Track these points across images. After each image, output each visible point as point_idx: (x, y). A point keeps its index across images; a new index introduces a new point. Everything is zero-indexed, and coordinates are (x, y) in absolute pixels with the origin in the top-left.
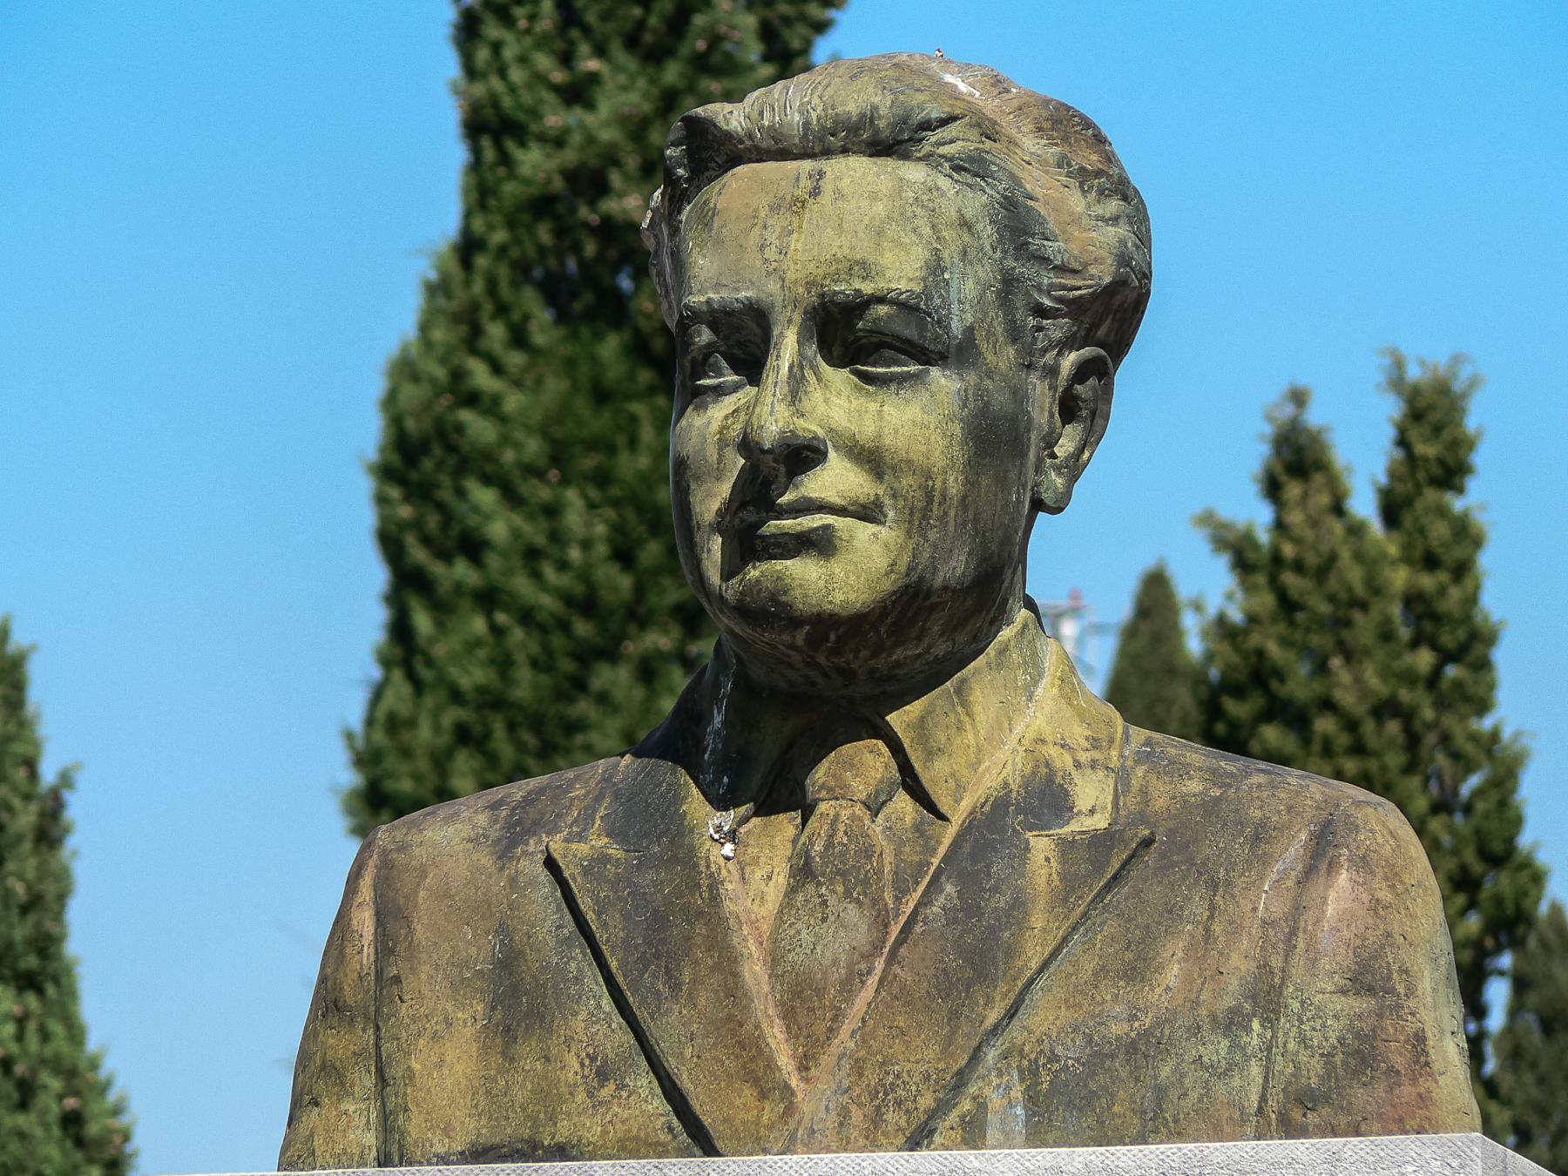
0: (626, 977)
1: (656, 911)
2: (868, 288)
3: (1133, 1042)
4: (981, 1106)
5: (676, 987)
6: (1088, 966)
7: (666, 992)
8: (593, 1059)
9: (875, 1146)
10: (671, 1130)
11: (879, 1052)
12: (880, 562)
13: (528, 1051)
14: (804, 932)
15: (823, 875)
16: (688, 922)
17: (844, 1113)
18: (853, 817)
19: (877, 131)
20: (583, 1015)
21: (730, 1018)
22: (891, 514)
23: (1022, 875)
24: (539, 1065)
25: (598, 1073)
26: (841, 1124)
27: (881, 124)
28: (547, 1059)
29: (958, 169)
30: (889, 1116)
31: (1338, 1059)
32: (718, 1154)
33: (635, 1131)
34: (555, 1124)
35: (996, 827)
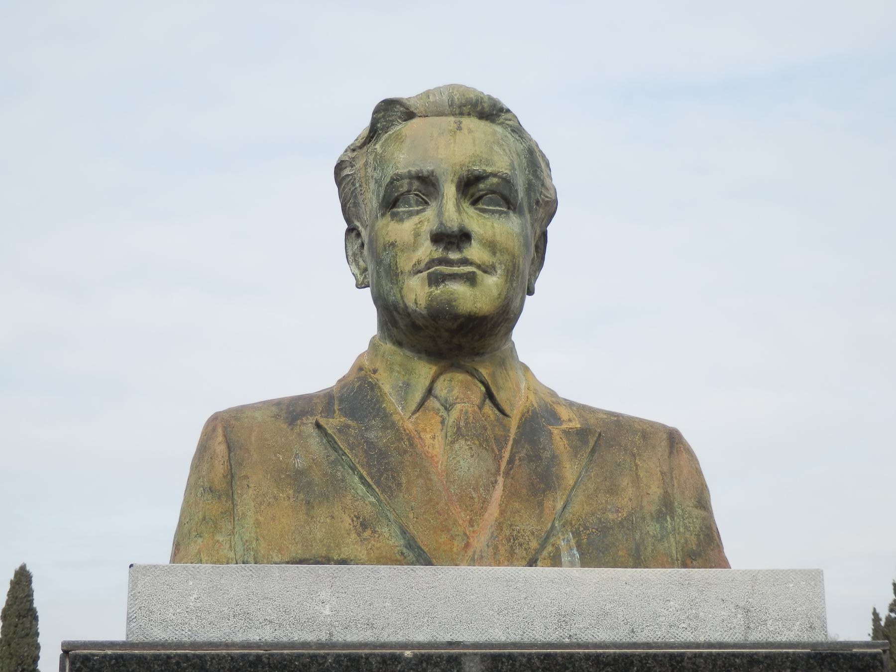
0: (372, 479)
1: (380, 450)
2: (489, 170)
3: (620, 522)
4: (558, 550)
5: (399, 485)
6: (591, 486)
7: (394, 487)
8: (358, 518)
9: (511, 564)
10: (402, 554)
11: (509, 519)
12: (495, 292)
13: (321, 512)
14: (462, 462)
15: (468, 435)
16: (400, 455)
17: (496, 548)
18: (474, 411)
19: (483, 108)
20: (349, 497)
21: (430, 500)
22: (499, 272)
23: (552, 444)
24: (328, 520)
25: (362, 524)
26: (495, 553)
27: (485, 105)
28: (333, 517)
29: (513, 131)
30: (517, 551)
31: (702, 536)
32: (432, 565)
33: (384, 554)
34: (340, 549)
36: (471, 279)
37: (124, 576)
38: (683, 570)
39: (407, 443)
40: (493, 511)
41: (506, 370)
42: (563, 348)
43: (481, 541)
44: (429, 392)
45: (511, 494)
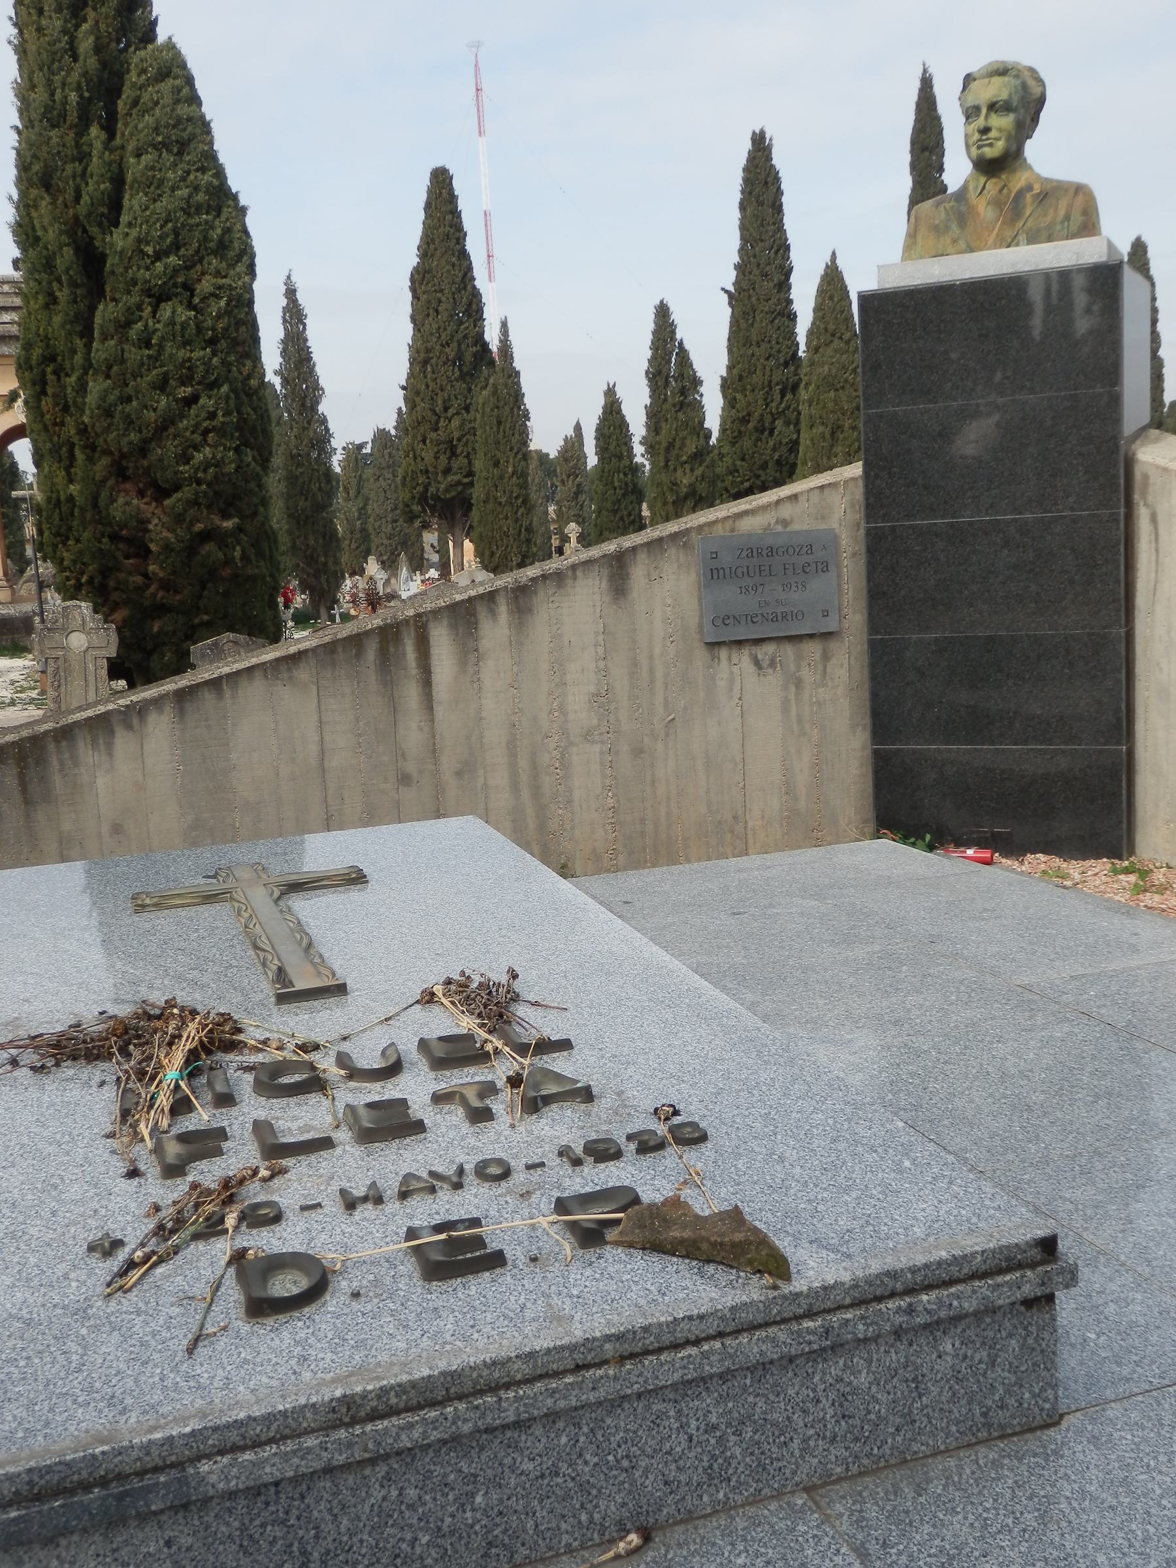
35: (1020, 194)
36: (991, 145)
37: (876, 269)
38: (811, 853)
39: (972, 209)
40: (996, 231)
41: (110, 754)
42: (1047, 155)
43: (990, 242)
44: (984, 188)
45: (1003, 223)
